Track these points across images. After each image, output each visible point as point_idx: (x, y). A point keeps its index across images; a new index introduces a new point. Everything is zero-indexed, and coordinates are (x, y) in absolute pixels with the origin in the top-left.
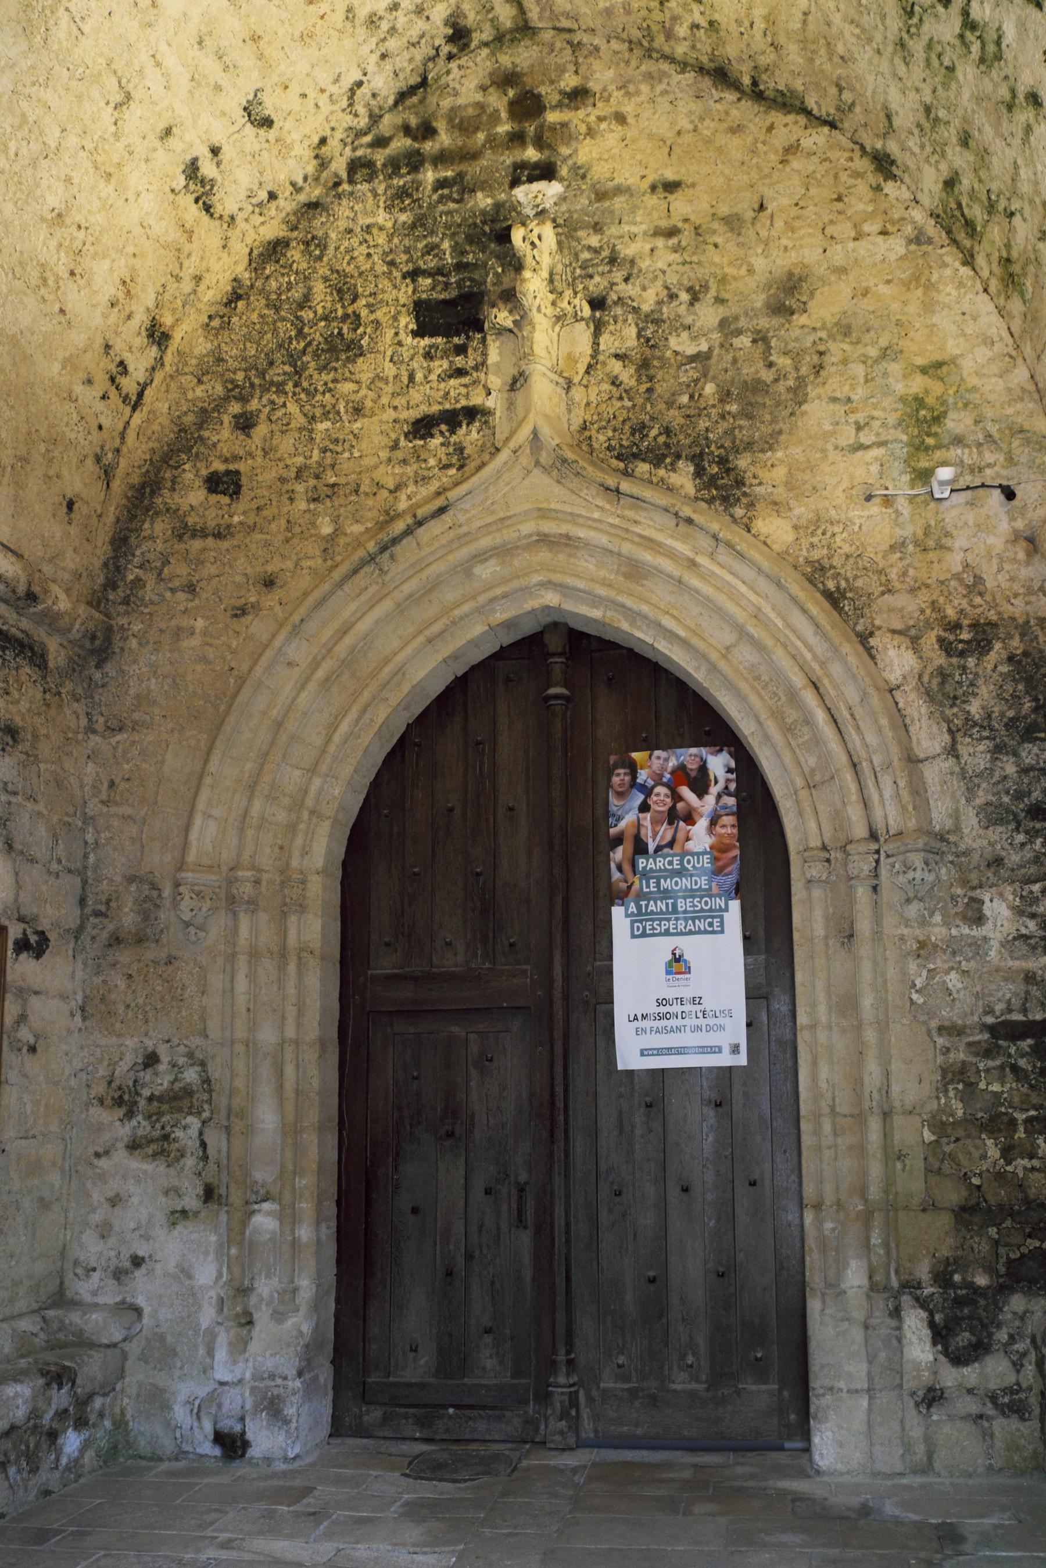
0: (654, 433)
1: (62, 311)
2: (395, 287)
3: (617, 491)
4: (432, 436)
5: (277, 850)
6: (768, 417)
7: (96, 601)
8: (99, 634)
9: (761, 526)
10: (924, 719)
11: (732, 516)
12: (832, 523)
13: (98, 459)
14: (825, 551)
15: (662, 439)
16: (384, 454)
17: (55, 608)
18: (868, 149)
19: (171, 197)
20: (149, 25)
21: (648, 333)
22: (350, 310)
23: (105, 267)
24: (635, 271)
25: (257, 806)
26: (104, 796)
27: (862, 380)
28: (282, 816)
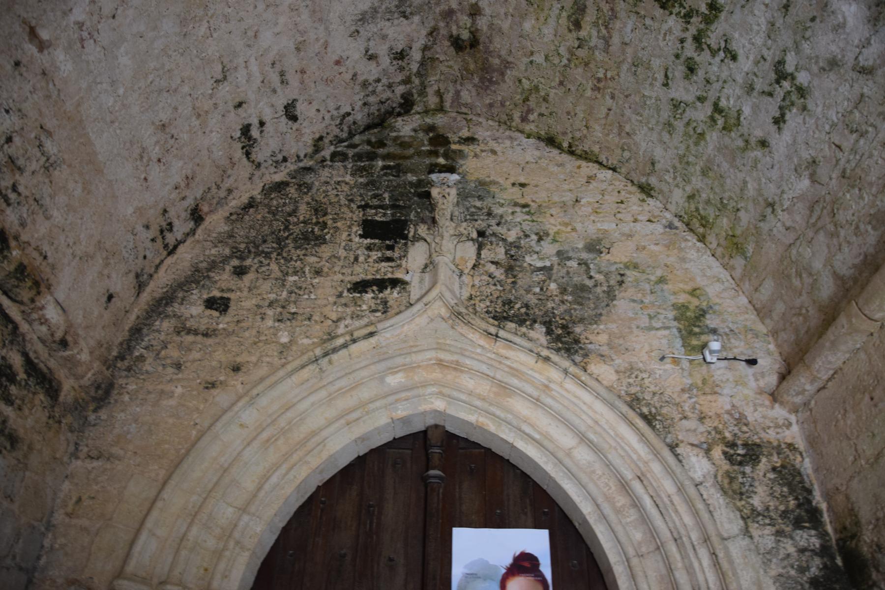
0: (517, 306)
1: (145, 179)
2: (352, 212)
3: (497, 336)
4: (366, 292)
5: (202, 571)
6: (592, 306)
7: (109, 364)
8: (103, 386)
9: (592, 368)
10: (723, 507)
11: (573, 361)
12: (641, 372)
13: (137, 276)
14: (638, 388)
15: (523, 310)
16: (332, 299)
17: (78, 356)
18: (636, 182)
19: (230, 140)
20: (249, 46)
21: (512, 253)
22: (321, 220)
23: (180, 165)
24: (503, 221)
25: (194, 530)
26: (69, 509)
27: (649, 292)
28: (211, 543)
